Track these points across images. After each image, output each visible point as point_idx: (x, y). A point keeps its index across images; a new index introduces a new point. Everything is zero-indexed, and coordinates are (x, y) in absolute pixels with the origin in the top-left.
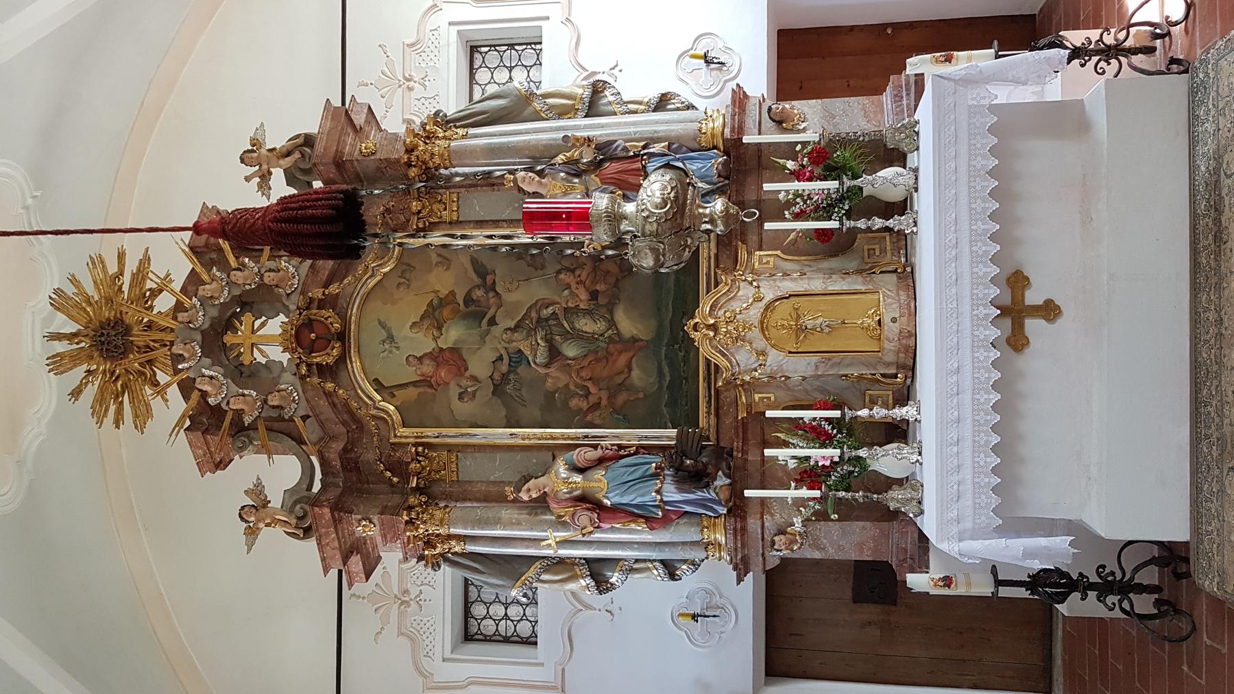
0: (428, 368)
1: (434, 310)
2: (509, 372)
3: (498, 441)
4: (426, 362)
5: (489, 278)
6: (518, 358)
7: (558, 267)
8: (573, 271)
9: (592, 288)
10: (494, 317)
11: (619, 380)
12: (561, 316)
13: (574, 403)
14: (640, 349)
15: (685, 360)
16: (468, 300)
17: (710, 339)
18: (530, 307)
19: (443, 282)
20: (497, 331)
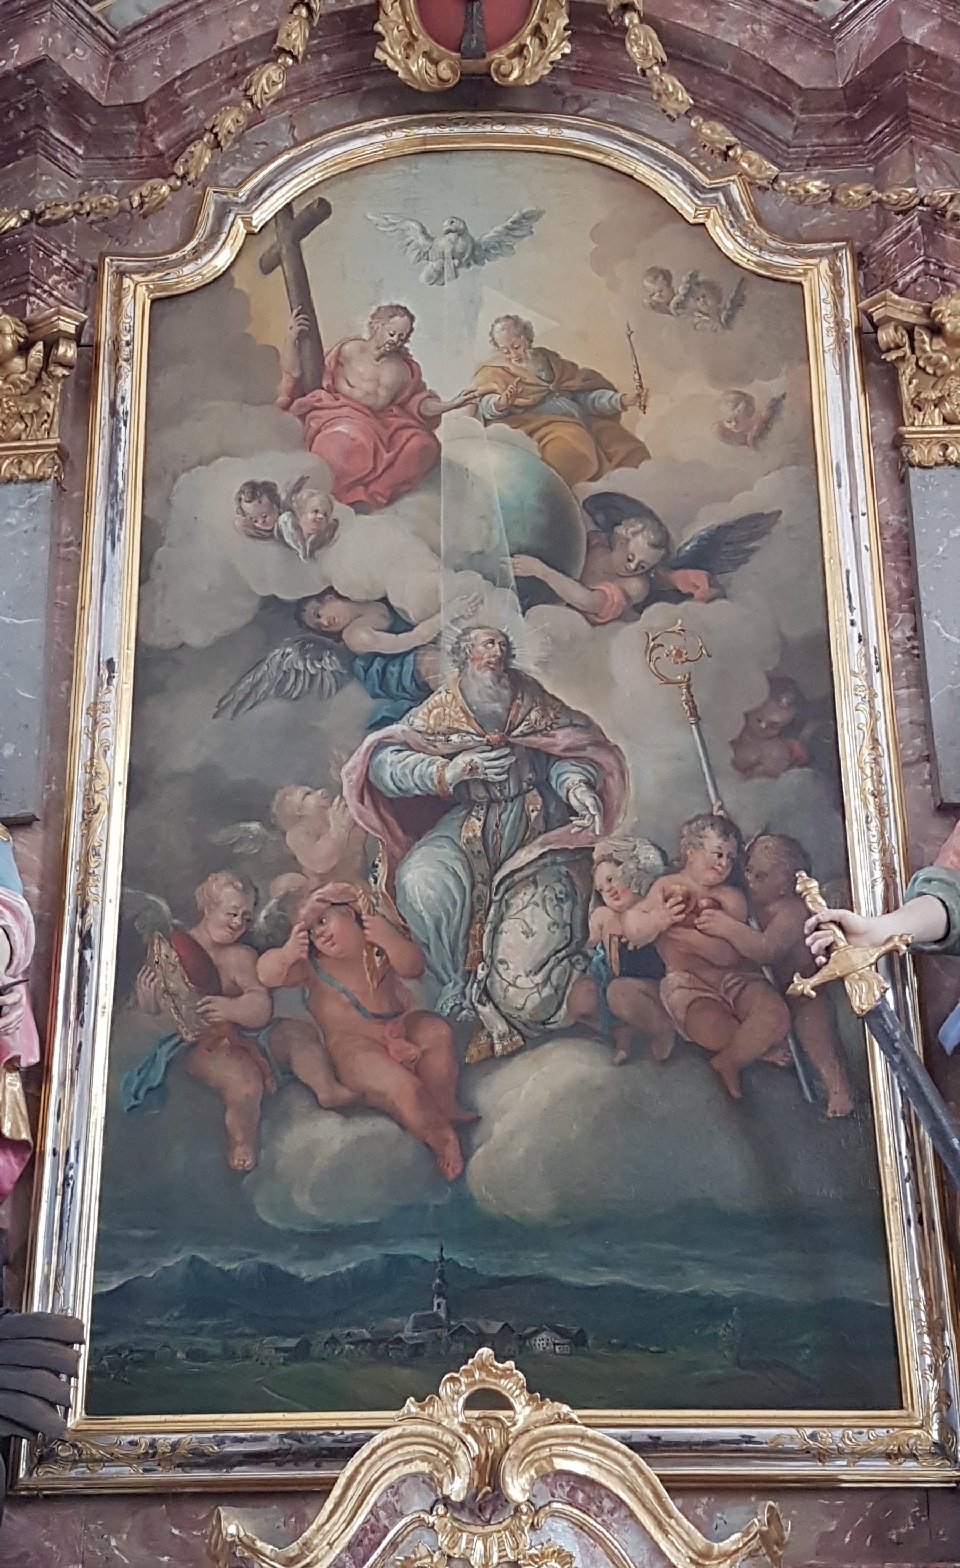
0: (366, 377)
1: (574, 396)
2: (348, 656)
3: (89, 619)
4: (389, 373)
5: (695, 579)
6: (397, 685)
7: (747, 826)
8: (735, 879)
9: (669, 955)
10: (552, 598)
11: (308, 1065)
12: (558, 837)
13: (224, 893)
14: (432, 1154)
15: (383, 1346)
16: (612, 510)
17: (430, 1482)
18: (588, 725)
19: (680, 431)
20: (502, 609)
